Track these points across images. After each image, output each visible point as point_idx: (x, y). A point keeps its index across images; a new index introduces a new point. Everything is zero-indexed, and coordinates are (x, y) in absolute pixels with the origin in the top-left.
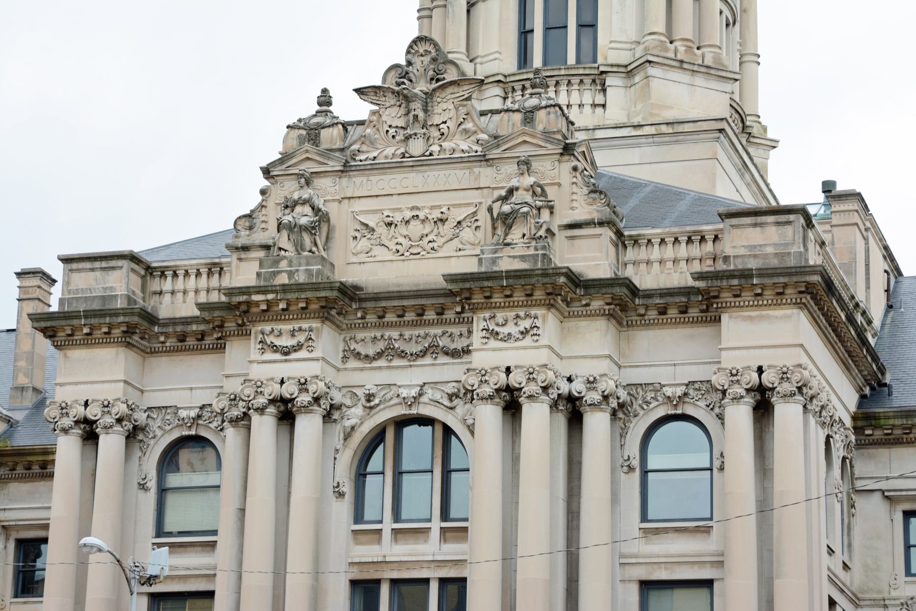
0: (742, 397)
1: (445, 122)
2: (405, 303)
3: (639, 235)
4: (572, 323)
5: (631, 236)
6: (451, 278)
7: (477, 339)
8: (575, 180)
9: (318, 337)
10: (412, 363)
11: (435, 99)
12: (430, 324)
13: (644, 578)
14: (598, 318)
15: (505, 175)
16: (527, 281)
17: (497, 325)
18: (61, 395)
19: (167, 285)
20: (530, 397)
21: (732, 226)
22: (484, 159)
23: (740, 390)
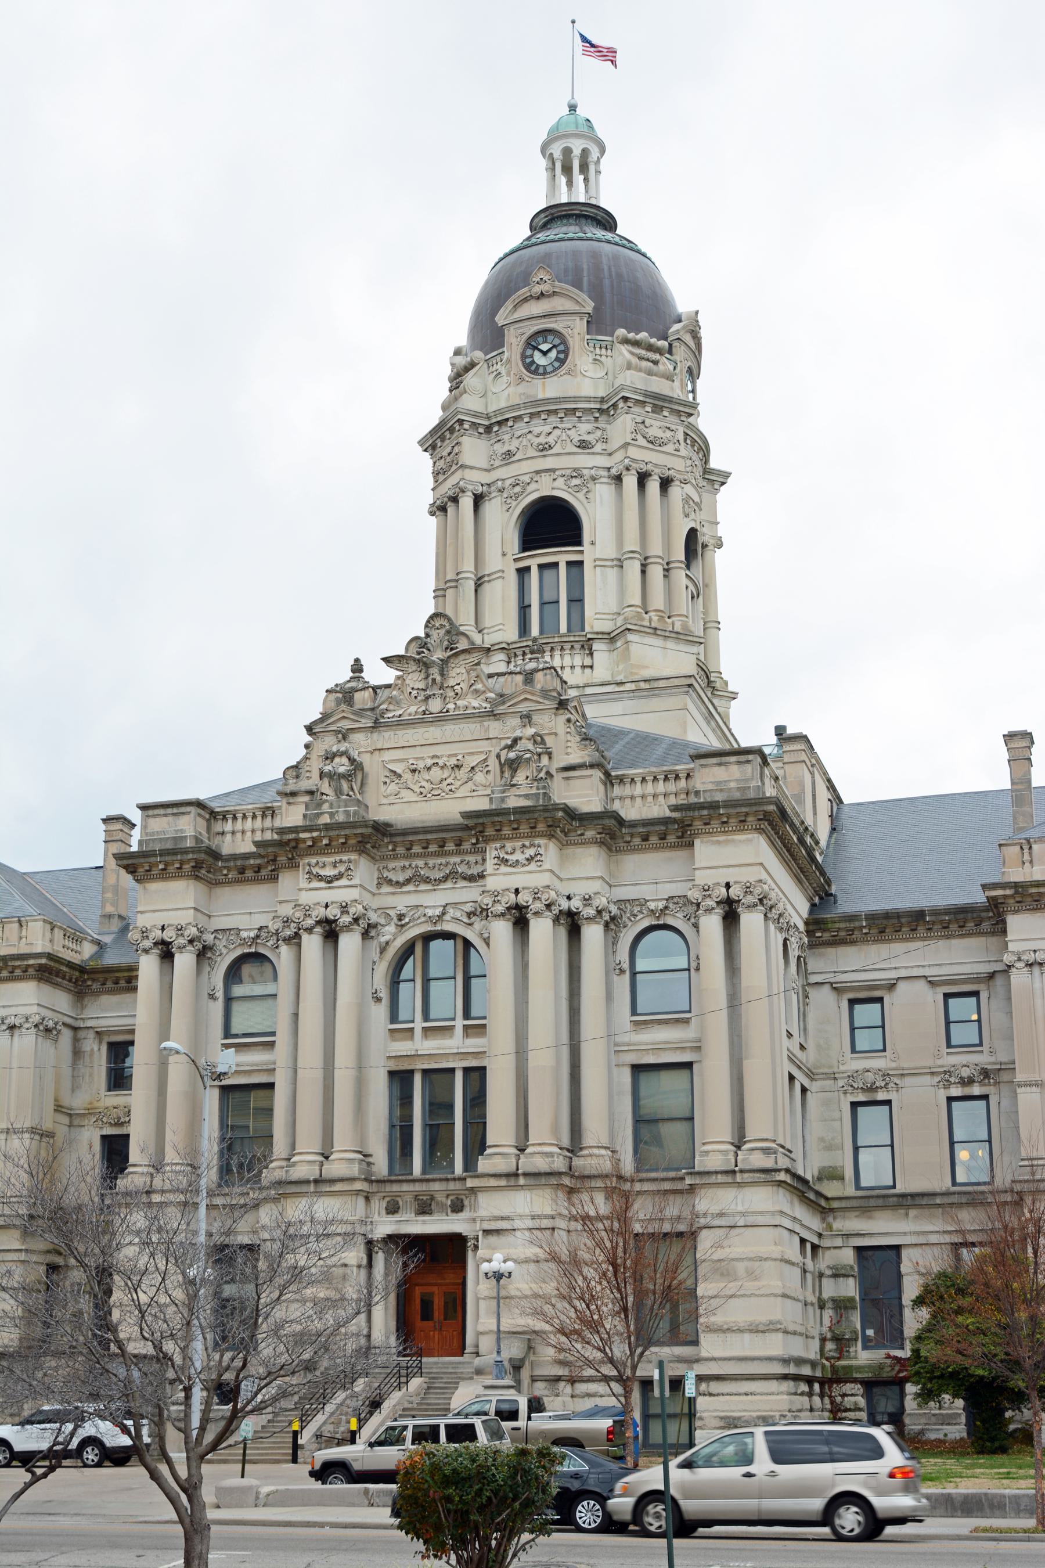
0: (713, 909)
2: (429, 837)
3: (624, 775)
4: (569, 850)
5: (617, 776)
7: (490, 866)
9: (356, 867)
13: (635, 1062)
15: (510, 727)
16: (531, 815)
17: (507, 853)
18: (142, 921)
19: (229, 826)
20: (536, 913)
22: (492, 715)
23: (711, 903)
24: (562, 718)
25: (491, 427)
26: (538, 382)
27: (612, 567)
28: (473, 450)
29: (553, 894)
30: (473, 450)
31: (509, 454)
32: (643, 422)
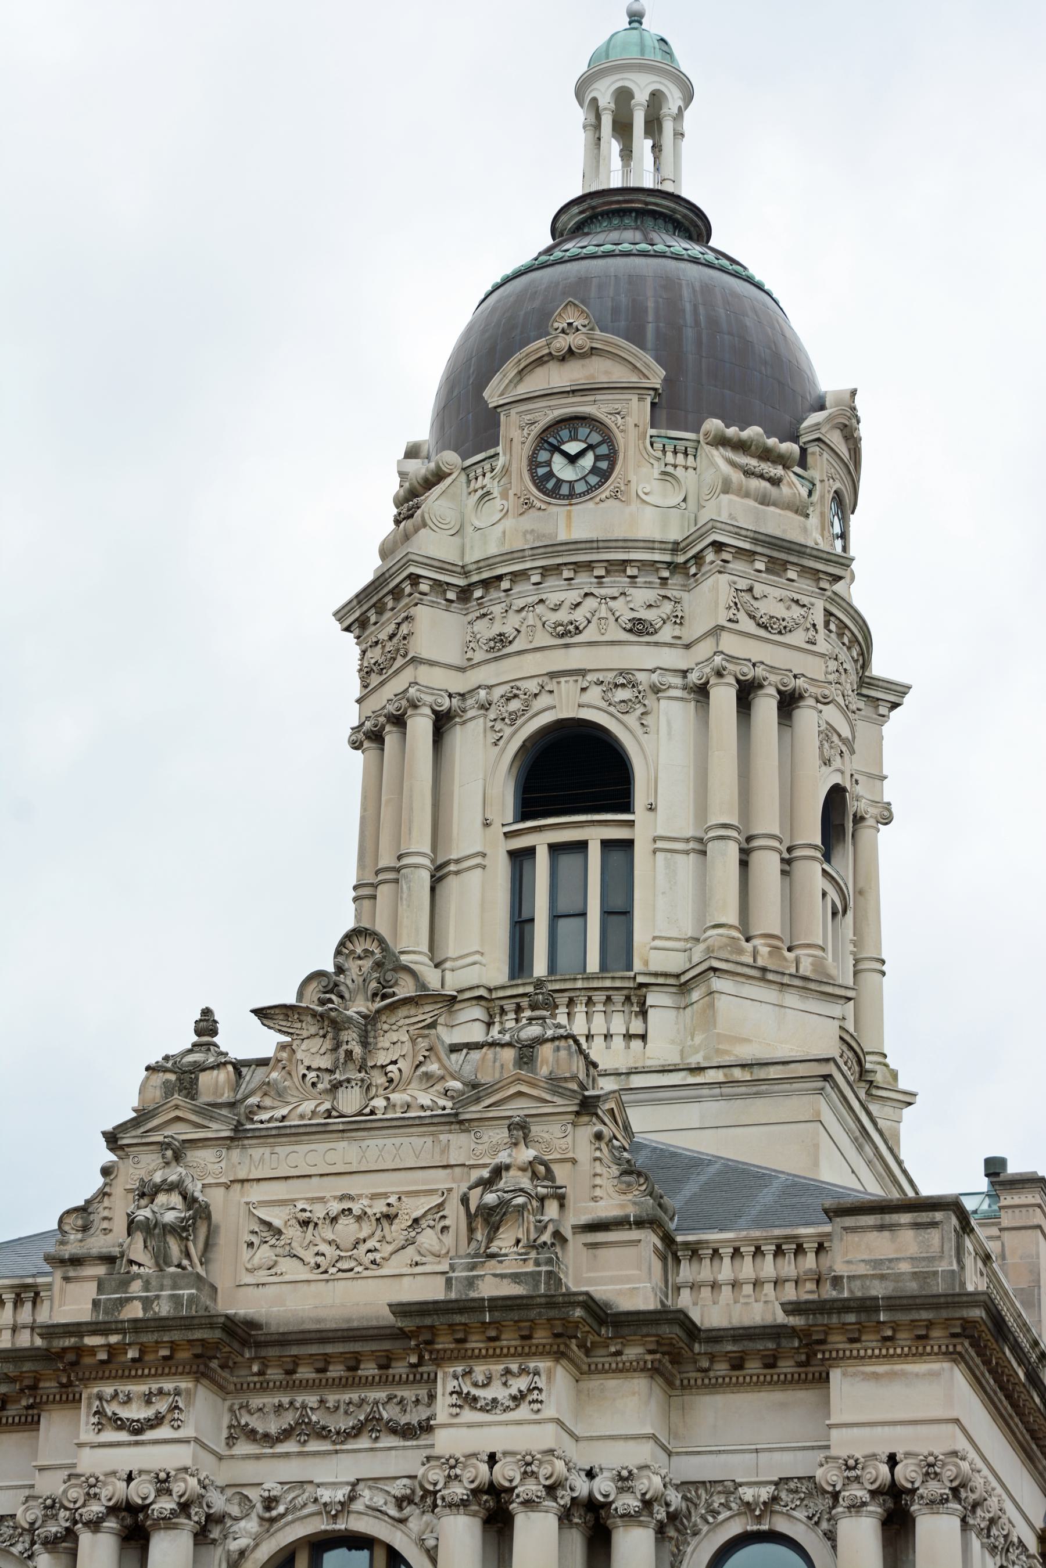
0: (864, 1504)
1: (395, 1062)
2: (329, 1349)
3: (699, 1242)
4: (594, 1383)
5: (686, 1244)
6: (400, 1309)
8: (598, 1154)
9: (188, 1404)
10: (338, 1447)
11: (379, 1025)
12: (369, 1383)
14: (636, 1374)
15: (491, 1146)
16: (523, 1314)
17: (475, 1385)
21: (845, 1229)
22: (456, 1121)
24: (586, 1132)
25: (470, 589)
26: (558, 511)
27: (687, 852)
28: (436, 631)
30: (436, 631)
31: (502, 639)
32: (750, 590)
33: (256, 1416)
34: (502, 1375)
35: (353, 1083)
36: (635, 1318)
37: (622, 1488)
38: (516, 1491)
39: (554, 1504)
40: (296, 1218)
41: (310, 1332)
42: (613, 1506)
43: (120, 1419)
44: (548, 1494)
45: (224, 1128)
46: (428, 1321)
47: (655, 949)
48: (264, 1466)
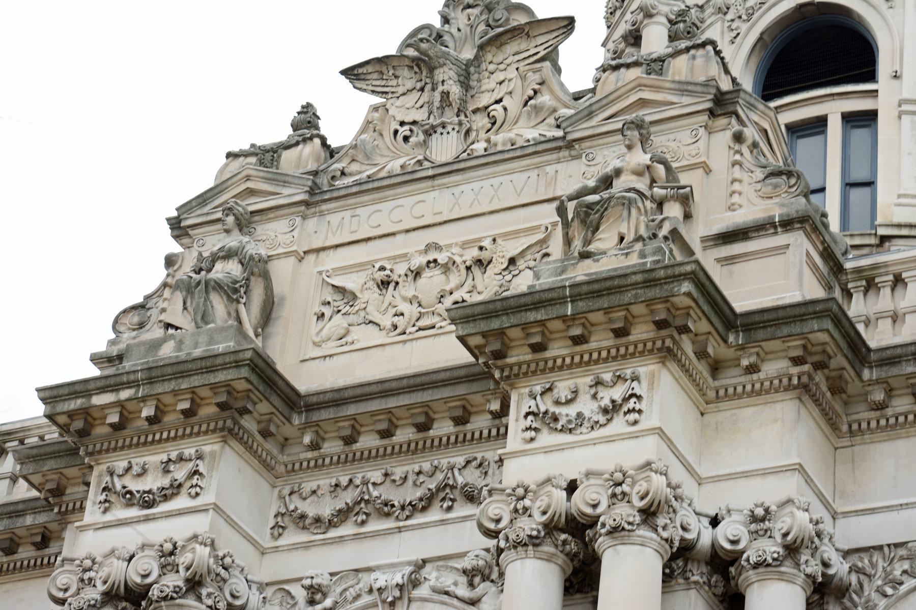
1: (500, 101)
2: (392, 402)
3: (875, 267)
4: (724, 415)
5: (858, 271)
8: (738, 157)
9: (211, 469)
10: (401, 524)
11: (483, 66)
12: (444, 444)
14: (779, 396)
16: (615, 299)
17: (557, 403)
20: (615, 530)
29: (658, 482)
33: (308, 501)
34: (591, 387)
35: (449, 128)
36: (772, 316)
37: (757, 532)
38: (601, 519)
39: (654, 536)
40: (374, 280)
41: (369, 384)
42: (745, 556)
43: (130, 492)
44: (644, 522)
45: (299, 191)
46: (495, 324)
47: (900, 205)
48: (315, 554)
